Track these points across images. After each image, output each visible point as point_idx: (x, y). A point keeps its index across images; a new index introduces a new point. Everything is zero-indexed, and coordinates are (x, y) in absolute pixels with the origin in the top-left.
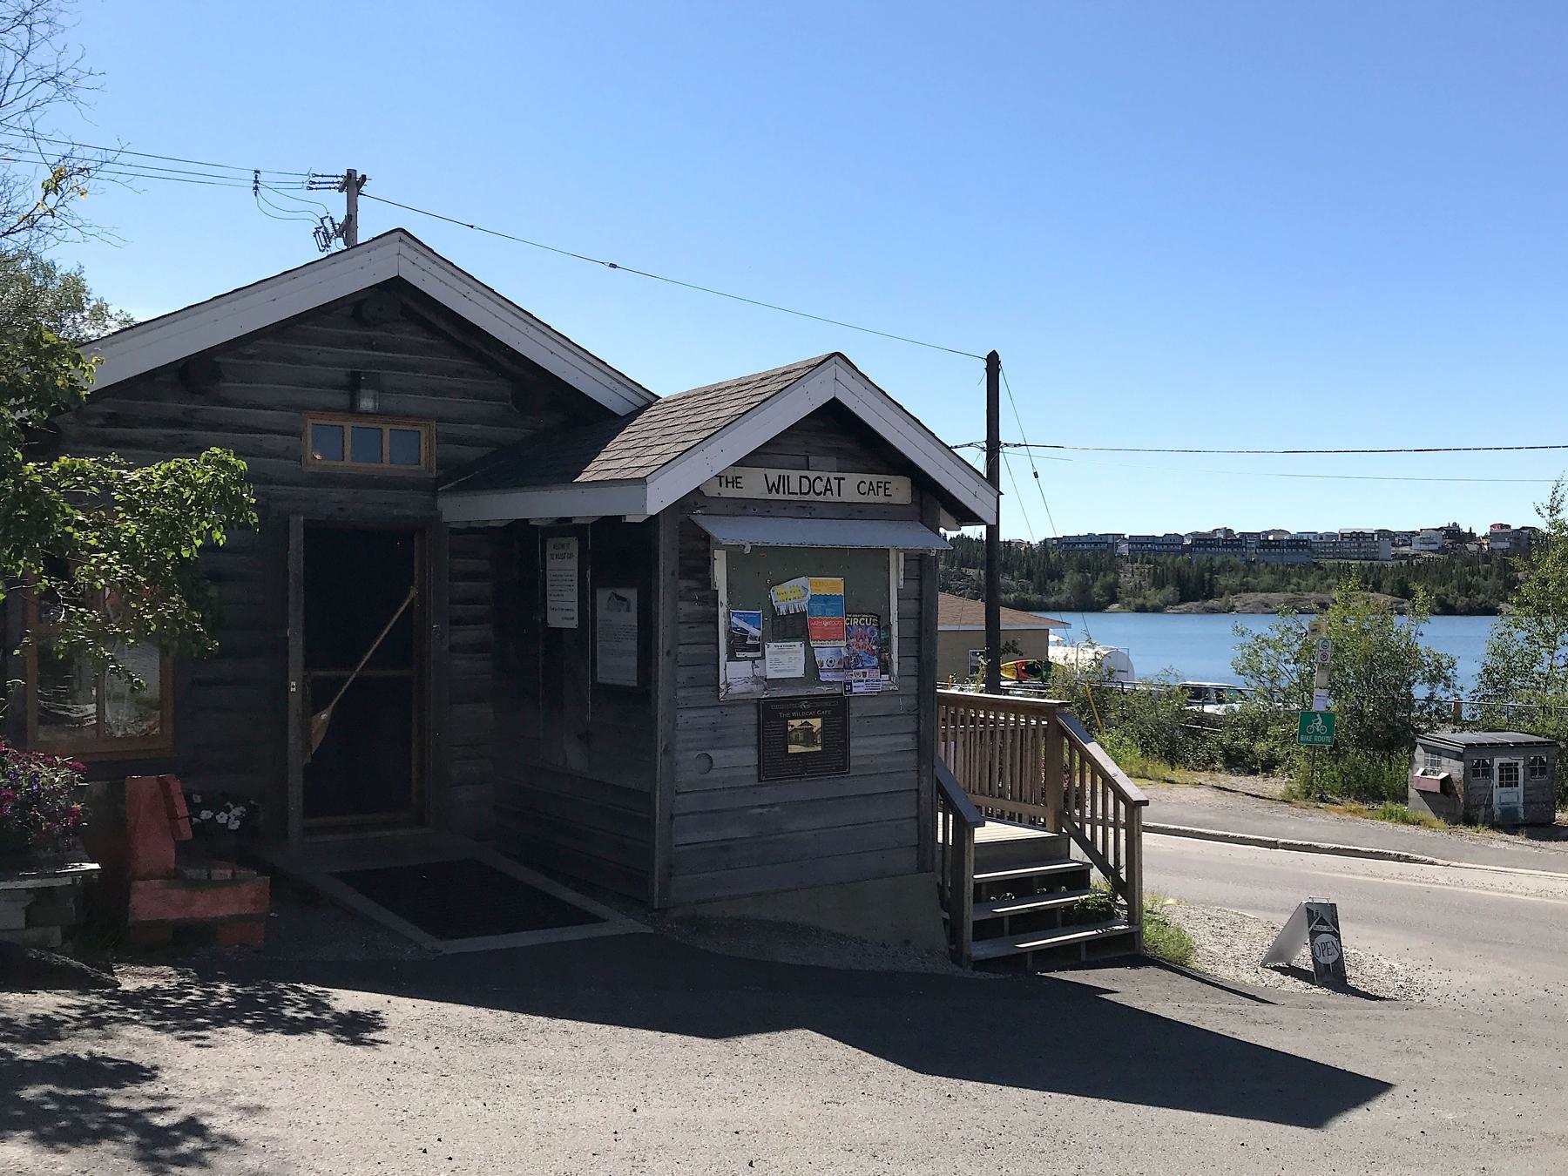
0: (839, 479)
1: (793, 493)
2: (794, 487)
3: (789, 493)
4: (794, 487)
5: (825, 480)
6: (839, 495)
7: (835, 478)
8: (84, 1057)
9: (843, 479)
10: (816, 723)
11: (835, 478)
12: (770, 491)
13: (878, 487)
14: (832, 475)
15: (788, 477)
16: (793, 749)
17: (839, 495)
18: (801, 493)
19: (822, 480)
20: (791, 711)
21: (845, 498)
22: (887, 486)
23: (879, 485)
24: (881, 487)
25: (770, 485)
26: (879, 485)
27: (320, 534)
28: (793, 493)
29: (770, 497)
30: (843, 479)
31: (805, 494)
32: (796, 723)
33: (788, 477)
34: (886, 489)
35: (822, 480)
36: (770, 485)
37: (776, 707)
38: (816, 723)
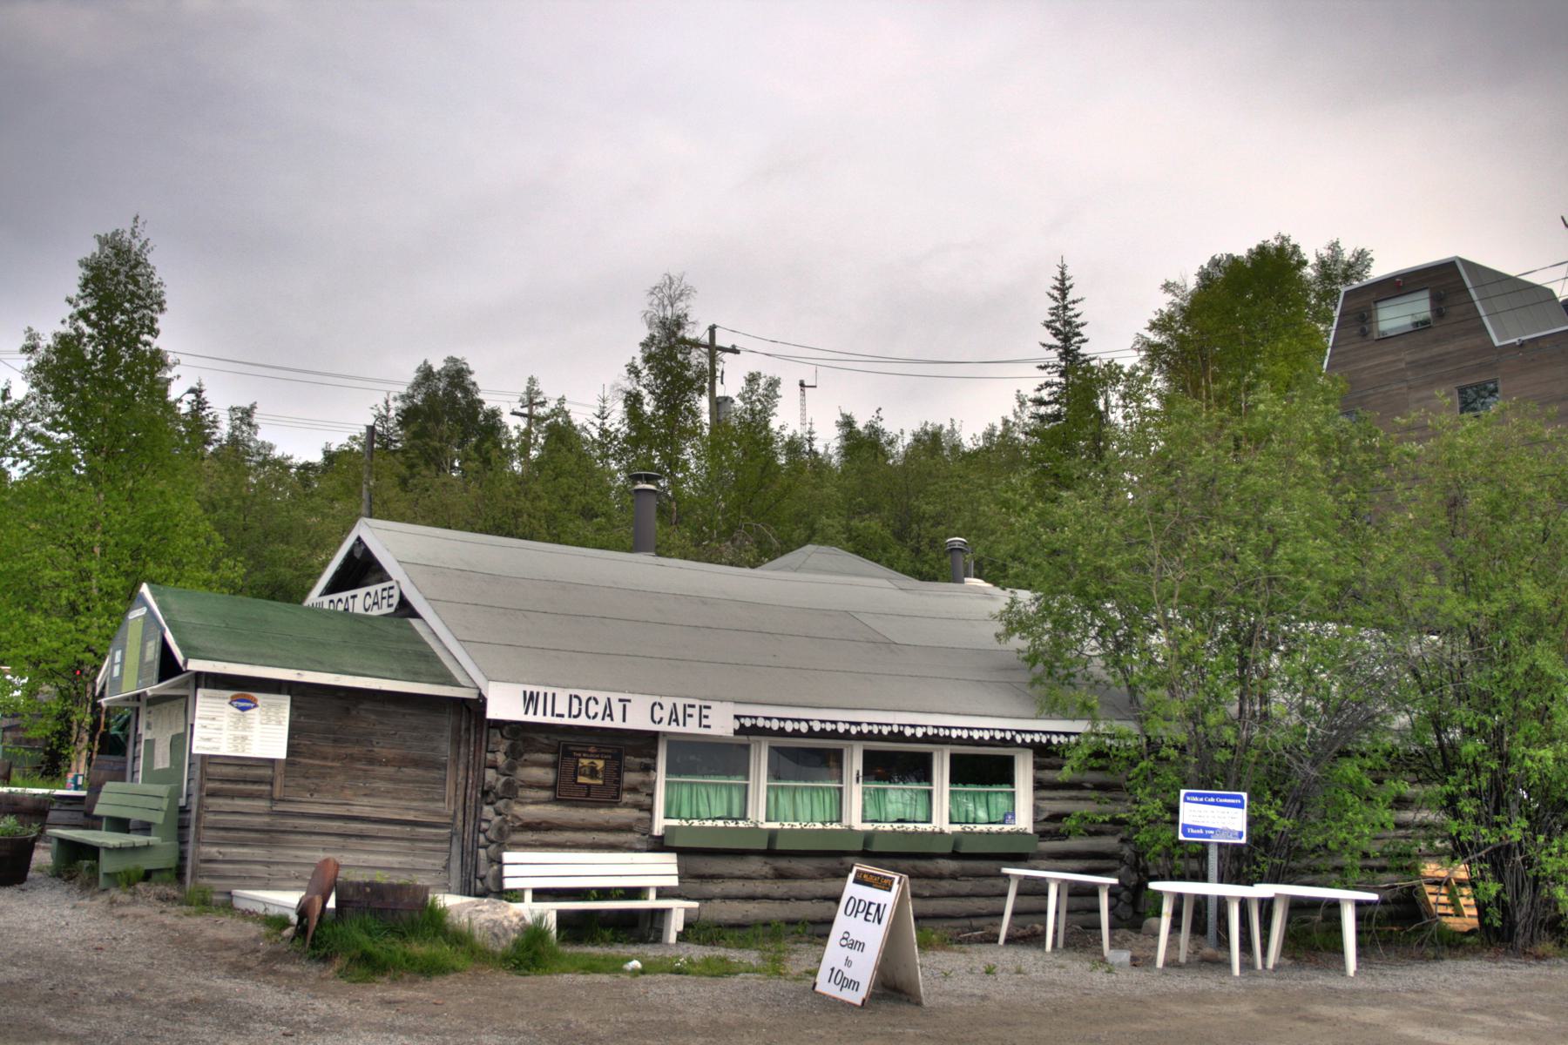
1: (559, 715)
2: (562, 707)
4: (562, 707)
5: (603, 702)
6: (624, 720)
7: (620, 700)
8: (828, 441)
9: (629, 701)
10: (600, 764)
11: (620, 700)
14: (615, 697)
15: (554, 695)
16: (582, 779)
17: (624, 720)
19: (597, 703)
20: (582, 752)
21: (631, 724)
22: (705, 712)
23: (689, 711)
24: (691, 716)
27: (59, 775)
28: (559, 715)
29: (530, 718)
30: (629, 701)
31: (575, 717)
32: (585, 762)
33: (554, 695)
35: (597, 703)
37: (572, 748)
38: (600, 764)
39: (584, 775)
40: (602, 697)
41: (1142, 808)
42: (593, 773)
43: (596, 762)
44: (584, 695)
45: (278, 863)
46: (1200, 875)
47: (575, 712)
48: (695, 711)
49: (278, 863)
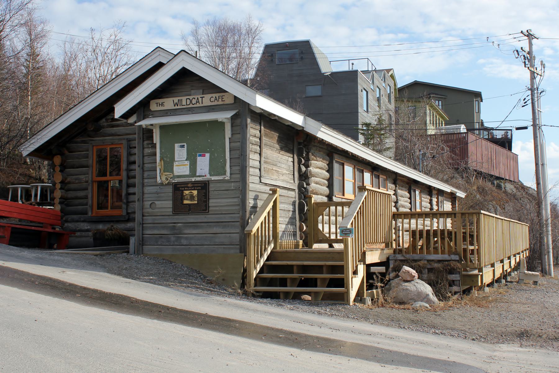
0: (202, 98)
3: (182, 105)
4: (184, 103)
6: (202, 103)
9: (204, 97)
10: (195, 192)
12: (175, 106)
13: (219, 98)
16: (186, 202)
17: (202, 103)
18: (187, 105)
20: (184, 187)
23: (220, 97)
25: (175, 104)
26: (220, 97)
30: (204, 97)
31: (188, 105)
32: (187, 192)
34: (222, 98)
36: (175, 104)
37: (179, 186)
38: (195, 192)
39: (187, 199)
40: (196, 97)
41: (372, 310)
42: (192, 198)
43: (192, 191)
44: (191, 97)
45: (491, 157)
46: (396, 216)
47: (188, 103)
48: (221, 97)
49: (491, 157)
